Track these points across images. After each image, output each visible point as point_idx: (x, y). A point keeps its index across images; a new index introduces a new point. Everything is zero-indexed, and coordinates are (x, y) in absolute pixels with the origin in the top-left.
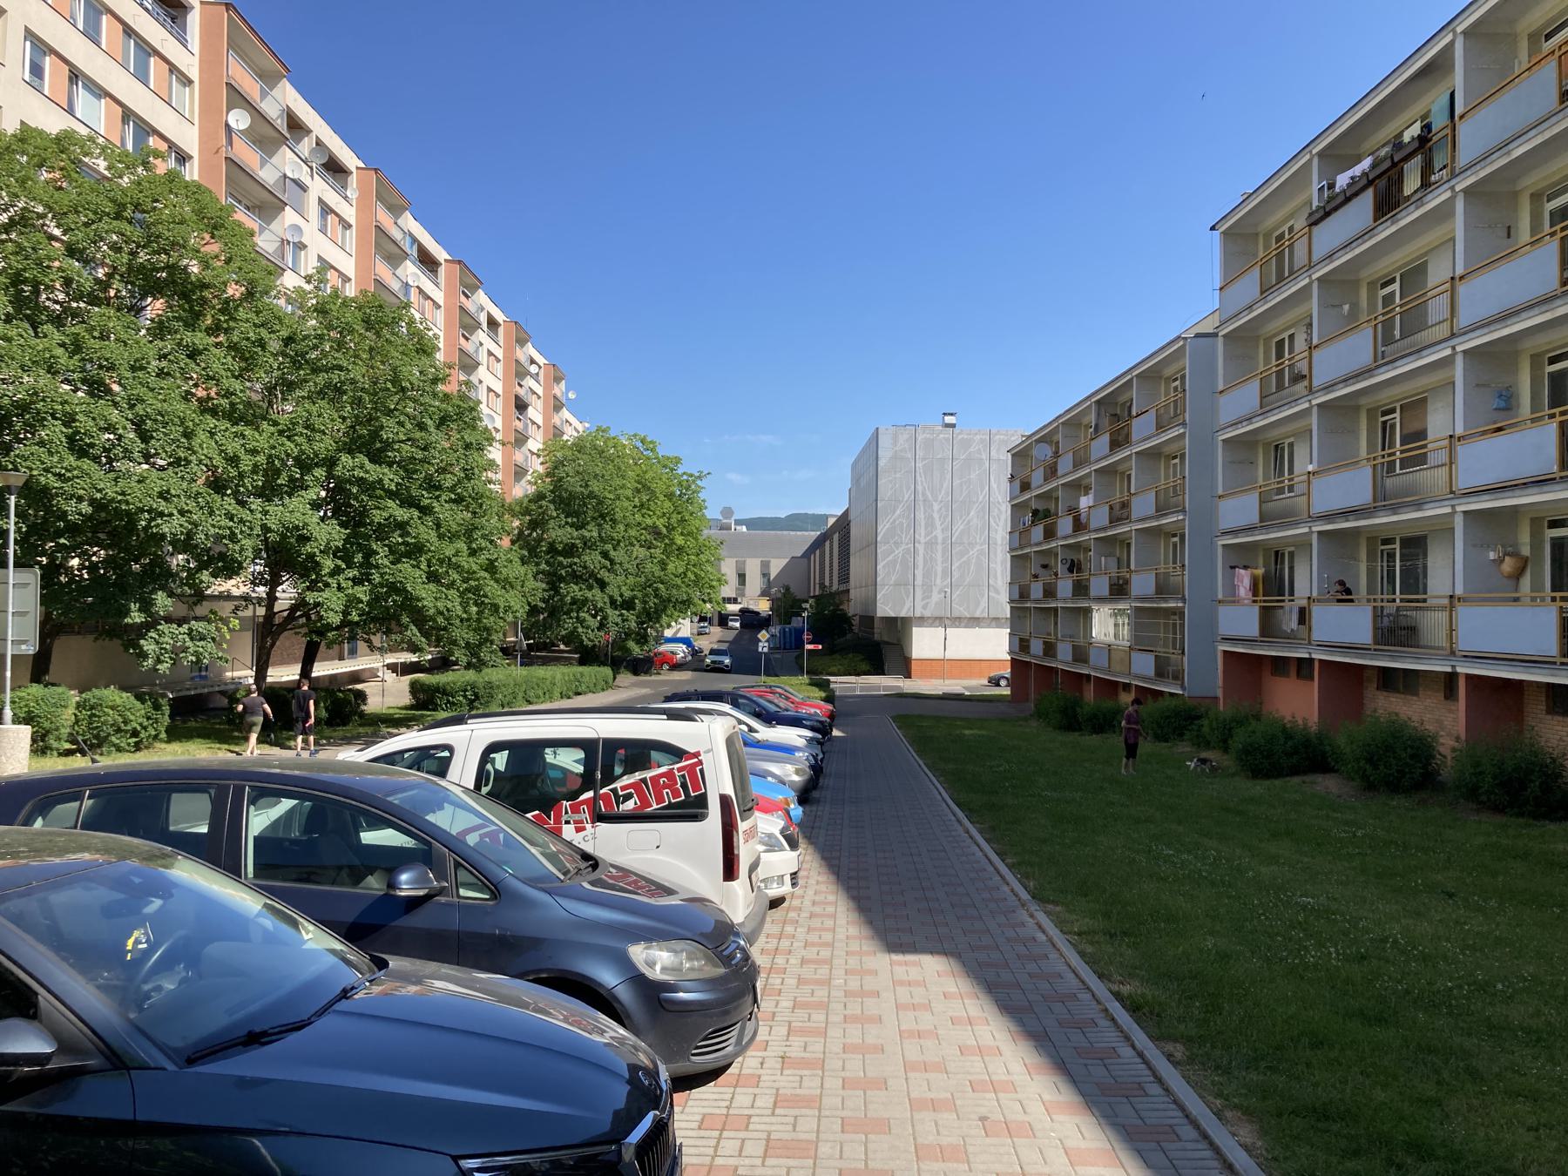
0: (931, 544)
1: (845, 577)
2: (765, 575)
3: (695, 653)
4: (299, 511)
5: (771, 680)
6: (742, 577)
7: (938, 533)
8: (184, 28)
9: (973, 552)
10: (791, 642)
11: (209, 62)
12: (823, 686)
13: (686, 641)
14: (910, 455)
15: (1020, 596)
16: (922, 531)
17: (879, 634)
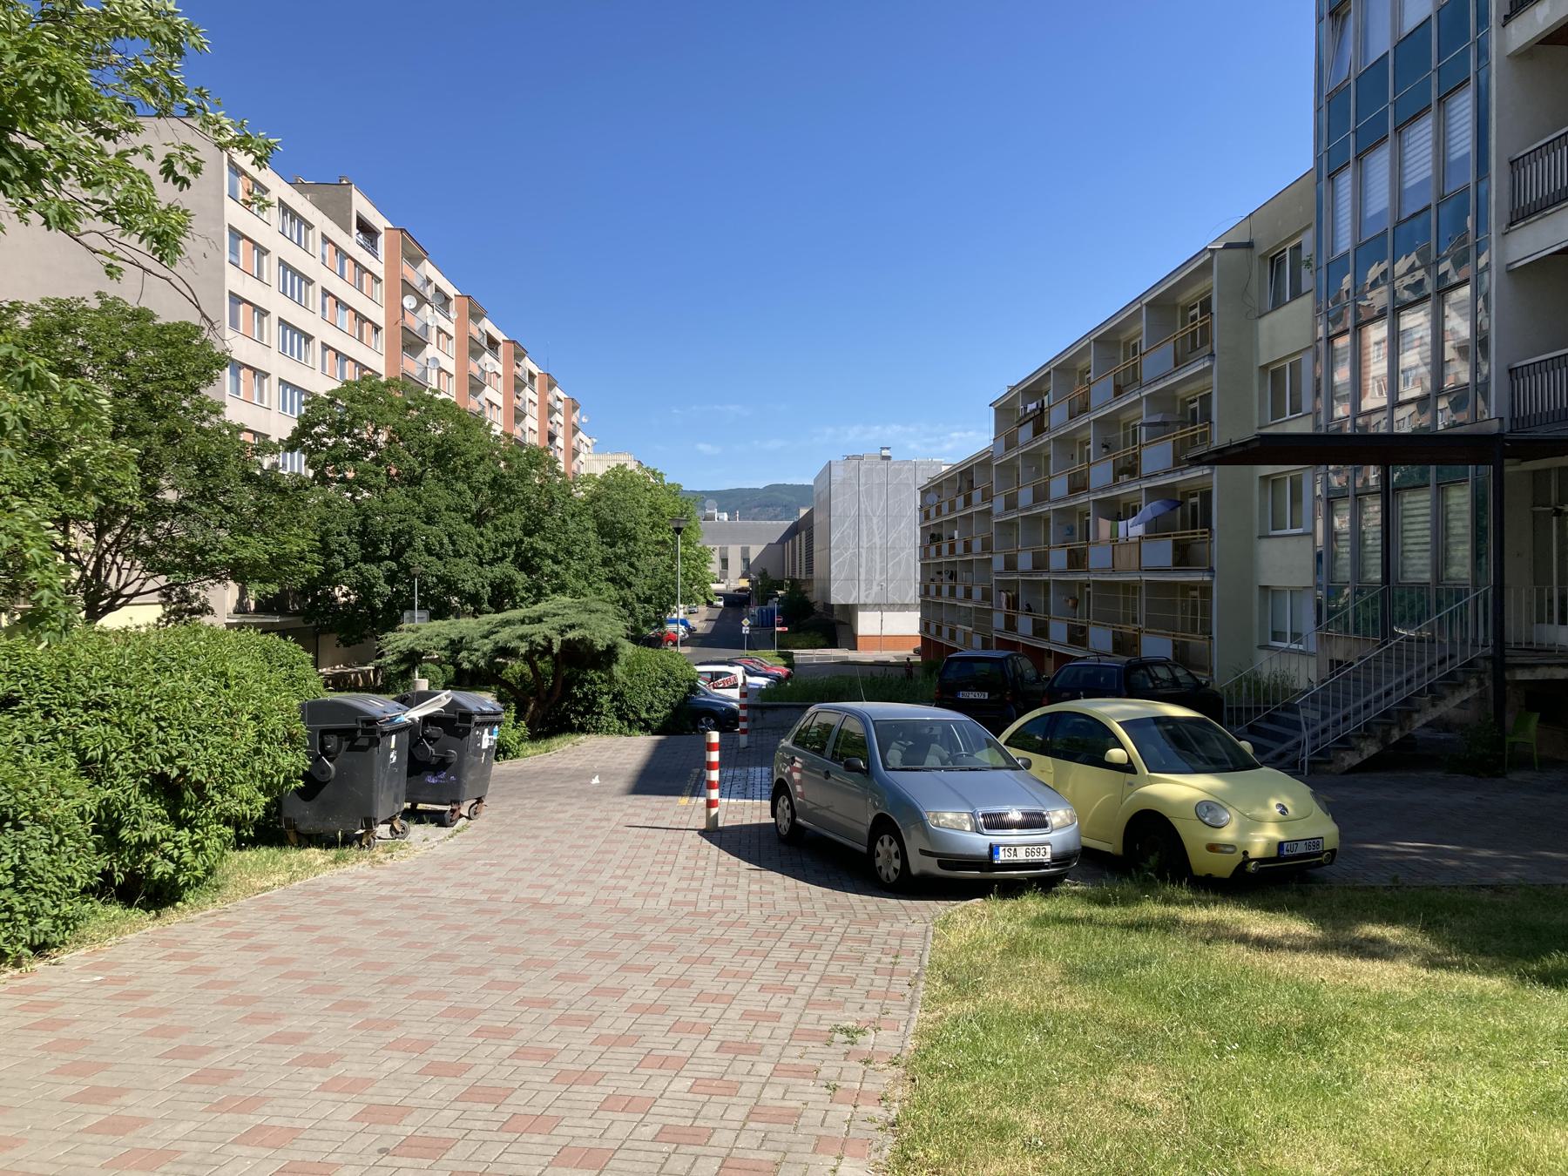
0: (871, 549)
1: (810, 569)
2: (746, 560)
3: (690, 630)
4: (507, 568)
5: (751, 653)
6: (725, 562)
7: (877, 540)
8: (375, 246)
9: (903, 555)
10: (765, 622)
11: (391, 266)
12: (788, 657)
13: (684, 622)
14: (855, 482)
15: (925, 592)
16: (864, 538)
17: (837, 616)
